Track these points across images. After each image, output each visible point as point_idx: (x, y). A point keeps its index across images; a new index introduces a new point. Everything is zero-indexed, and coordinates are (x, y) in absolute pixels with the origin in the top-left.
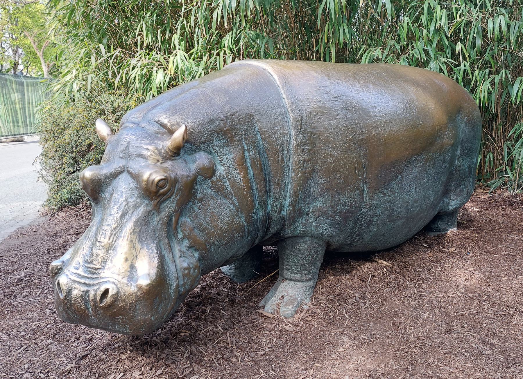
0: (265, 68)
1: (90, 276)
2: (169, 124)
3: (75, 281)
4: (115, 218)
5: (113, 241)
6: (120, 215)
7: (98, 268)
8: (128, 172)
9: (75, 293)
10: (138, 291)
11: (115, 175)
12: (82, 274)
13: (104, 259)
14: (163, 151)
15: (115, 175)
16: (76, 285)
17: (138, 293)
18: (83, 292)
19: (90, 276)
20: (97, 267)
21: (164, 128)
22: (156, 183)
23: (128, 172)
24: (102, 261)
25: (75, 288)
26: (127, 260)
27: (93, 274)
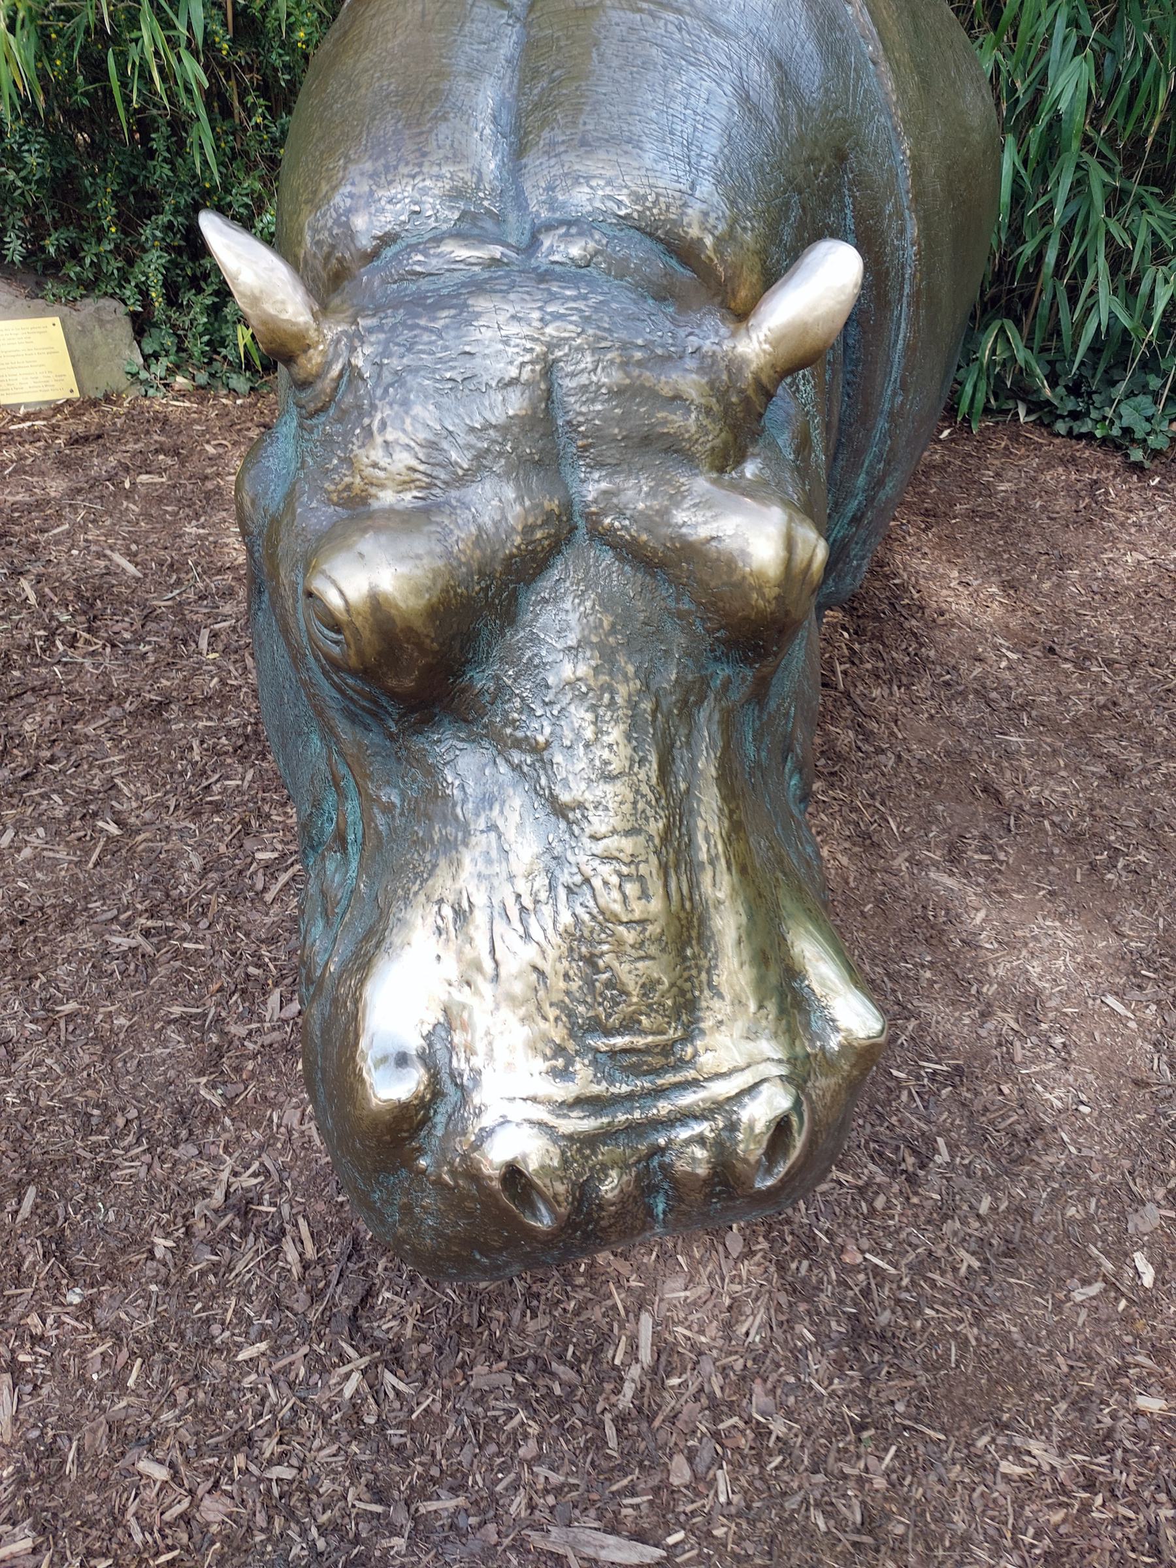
4: (645, 789)
6: (655, 766)
14: (734, 399)
27: (657, 1072)
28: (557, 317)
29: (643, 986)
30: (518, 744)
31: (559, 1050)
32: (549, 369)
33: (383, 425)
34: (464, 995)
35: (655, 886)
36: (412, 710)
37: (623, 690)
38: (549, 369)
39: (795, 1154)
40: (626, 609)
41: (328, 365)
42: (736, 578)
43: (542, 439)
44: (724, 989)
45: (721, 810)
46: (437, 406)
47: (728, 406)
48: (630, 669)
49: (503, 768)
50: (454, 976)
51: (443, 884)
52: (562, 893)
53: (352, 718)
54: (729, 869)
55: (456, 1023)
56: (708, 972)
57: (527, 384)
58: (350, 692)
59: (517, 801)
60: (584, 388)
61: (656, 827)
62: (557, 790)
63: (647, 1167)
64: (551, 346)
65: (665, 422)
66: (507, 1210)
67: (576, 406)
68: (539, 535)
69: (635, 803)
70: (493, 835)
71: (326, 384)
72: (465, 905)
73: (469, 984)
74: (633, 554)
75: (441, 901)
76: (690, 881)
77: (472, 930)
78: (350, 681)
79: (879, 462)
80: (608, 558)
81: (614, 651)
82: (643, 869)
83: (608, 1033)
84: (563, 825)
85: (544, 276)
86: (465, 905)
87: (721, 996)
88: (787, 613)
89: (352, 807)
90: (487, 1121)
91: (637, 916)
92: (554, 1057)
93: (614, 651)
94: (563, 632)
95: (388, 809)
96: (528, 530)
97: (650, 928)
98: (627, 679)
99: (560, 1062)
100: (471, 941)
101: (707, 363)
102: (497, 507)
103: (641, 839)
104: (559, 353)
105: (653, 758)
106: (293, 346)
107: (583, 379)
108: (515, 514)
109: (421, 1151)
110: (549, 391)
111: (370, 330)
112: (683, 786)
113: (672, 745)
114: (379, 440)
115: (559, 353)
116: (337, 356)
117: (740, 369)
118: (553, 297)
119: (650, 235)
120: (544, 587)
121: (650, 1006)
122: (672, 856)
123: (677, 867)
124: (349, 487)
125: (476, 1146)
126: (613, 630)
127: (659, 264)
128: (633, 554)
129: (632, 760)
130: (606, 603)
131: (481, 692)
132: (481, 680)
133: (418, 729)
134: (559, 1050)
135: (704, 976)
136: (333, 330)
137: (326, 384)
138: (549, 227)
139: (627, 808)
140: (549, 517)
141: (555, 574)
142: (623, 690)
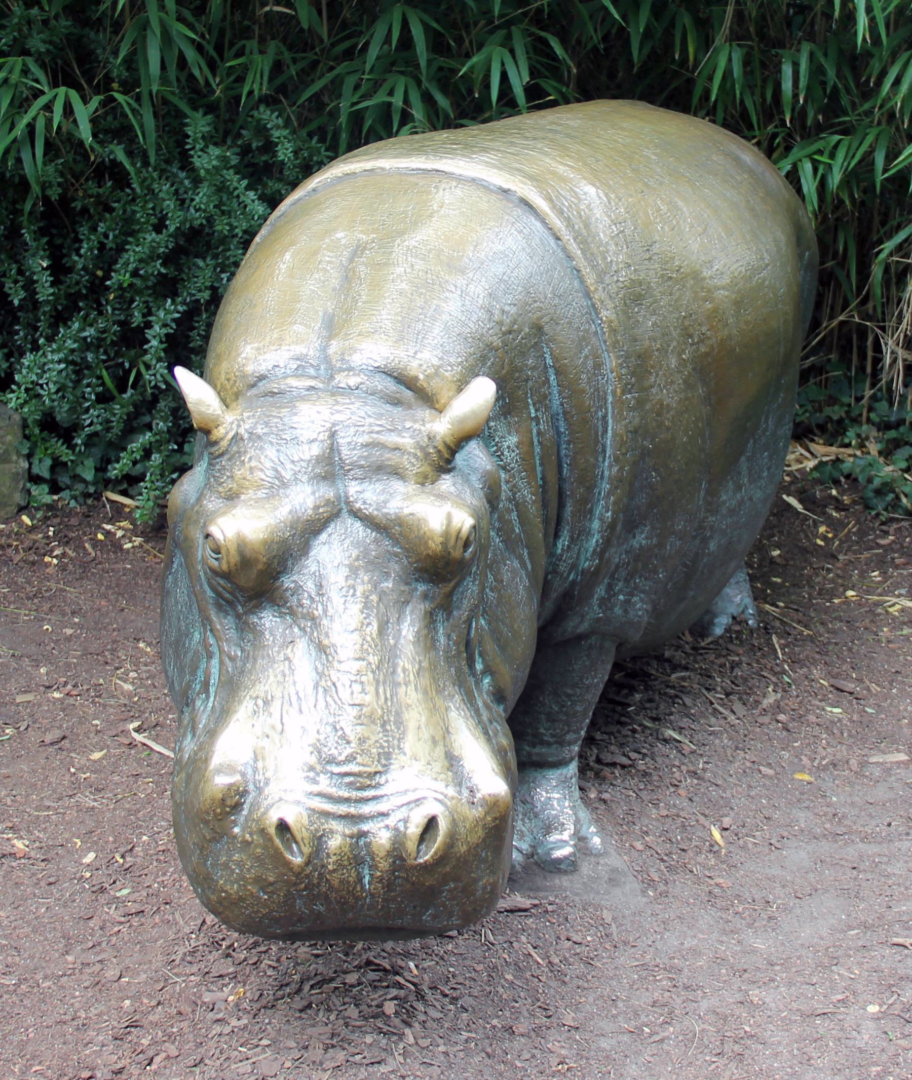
0: (505, 186)
1: (354, 794)
2: (421, 377)
3: (327, 814)
4: (369, 639)
5: (386, 699)
6: (376, 628)
7: (376, 773)
8: (356, 514)
9: (334, 843)
10: (487, 813)
11: (311, 529)
12: (333, 791)
13: (382, 747)
14: (431, 451)
15: (311, 529)
16: (335, 825)
17: (489, 818)
18: (351, 837)
19: (354, 794)
20: (372, 770)
21: (409, 388)
22: (464, 538)
23: (356, 514)
24: (379, 754)
25: (332, 832)
26: (434, 742)
27: (363, 788)
28: (338, 412)
29: (360, 739)
30: (304, 617)
31: (312, 768)
32: (333, 435)
33: (250, 459)
34: (265, 742)
35: (371, 689)
36: (250, 599)
37: (360, 589)
38: (333, 435)
39: (440, 839)
40: (366, 549)
41: (227, 433)
42: (422, 532)
43: (330, 467)
44: (407, 750)
45: (414, 659)
46: (278, 451)
47: (427, 454)
48: (366, 578)
49: (296, 630)
50: (260, 734)
51: (260, 689)
52: (321, 690)
53: (219, 607)
54: (416, 689)
55: (260, 757)
56: (399, 740)
57: (322, 441)
58: (220, 589)
59: (302, 645)
60: (349, 443)
61: (374, 659)
62: (322, 638)
63: (357, 842)
64: (334, 425)
65: (389, 459)
66: (277, 849)
67: (345, 452)
68: (321, 510)
69: (362, 645)
70: (287, 663)
71: (224, 443)
72: (269, 698)
73: (268, 736)
74: (369, 521)
75: (257, 697)
76: (391, 691)
77: (272, 710)
78: (222, 582)
79: (607, 511)
80: (358, 524)
81: (357, 569)
82: (364, 679)
83: (338, 764)
84: (324, 657)
85: (337, 392)
86: (269, 698)
87: (405, 754)
88: (449, 553)
89: (215, 662)
90: (269, 801)
91: (357, 702)
92: (309, 771)
93: (357, 569)
94: (333, 560)
95: (232, 659)
96: (316, 508)
97: (365, 709)
98: (363, 583)
99: (312, 774)
100: (271, 715)
101: (415, 433)
102: (303, 498)
103: (365, 663)
104: (337, 428)
105: (375, 625)
106: (212, 425)
107: (349, 440)
108: (310, 503)
109: (235, 823)
110: (332, 444)
111: (248, 418)
112: (392, 642)
113: (388, 622)
114: (247, 465)
115: (337, 428)
116: (232, 429)
117: (434, 437)
118: (337, 403)
119: (390, 375)
120: (323, 537)
121: (362, 750)
122: (382, 677)
123: (384, 683)
124: (230, 490)
125: (265, 813)
126: (357, 559)
127: (391, 386)
128: (369, 521)
129: (363, 623)
130: (356, 544)
131: (286, 590)
132: (287, 582)
133: (251, 612)
134: (312, 768)
135: (396, 742)
136: (229, 418)
137: (224, 443)
138: (341, 370)
139: (358, 647)
140: (328, 502)
141: (329, 530)
142: (360, 589)
